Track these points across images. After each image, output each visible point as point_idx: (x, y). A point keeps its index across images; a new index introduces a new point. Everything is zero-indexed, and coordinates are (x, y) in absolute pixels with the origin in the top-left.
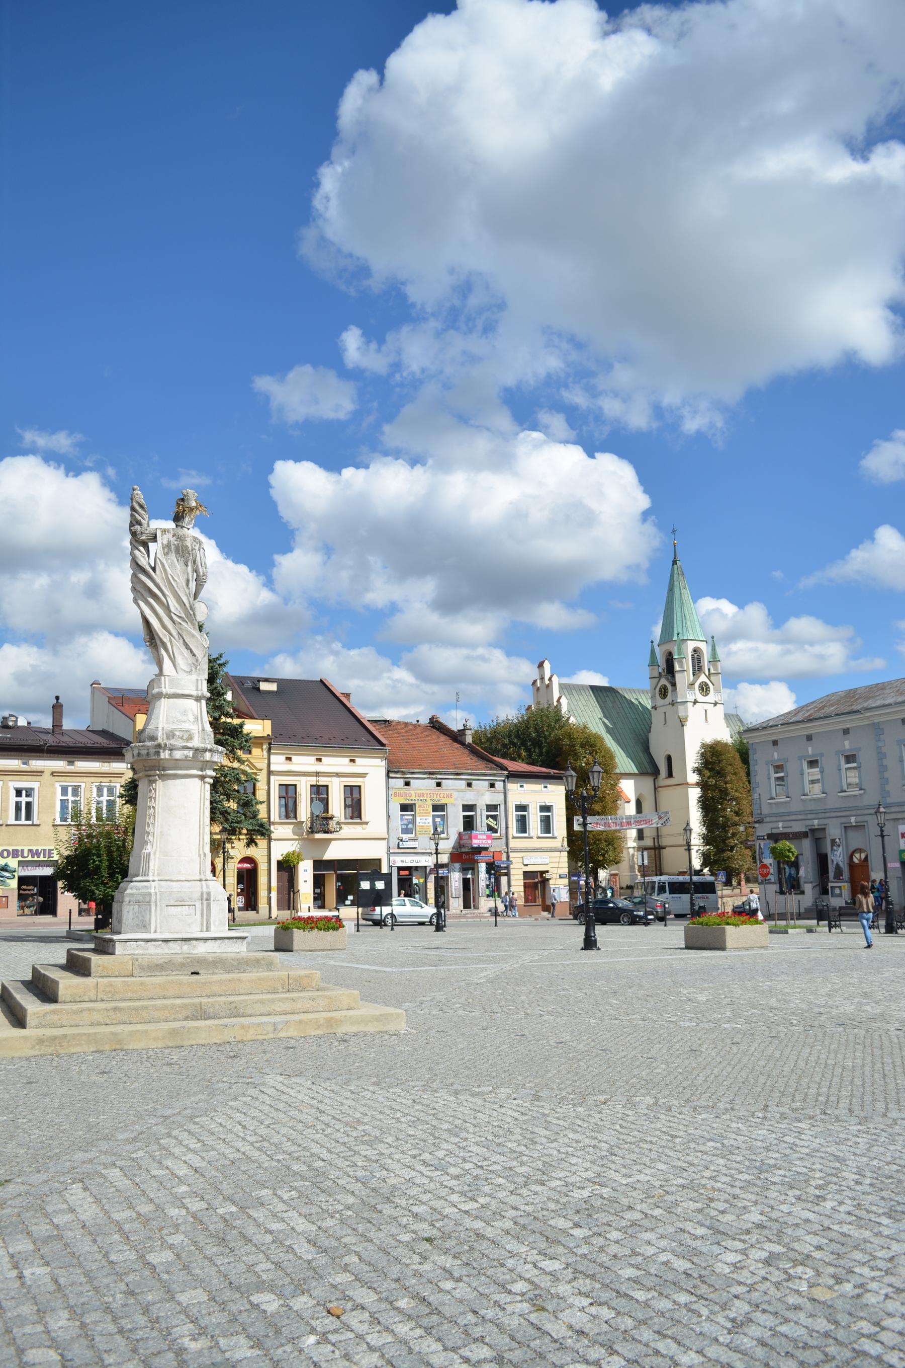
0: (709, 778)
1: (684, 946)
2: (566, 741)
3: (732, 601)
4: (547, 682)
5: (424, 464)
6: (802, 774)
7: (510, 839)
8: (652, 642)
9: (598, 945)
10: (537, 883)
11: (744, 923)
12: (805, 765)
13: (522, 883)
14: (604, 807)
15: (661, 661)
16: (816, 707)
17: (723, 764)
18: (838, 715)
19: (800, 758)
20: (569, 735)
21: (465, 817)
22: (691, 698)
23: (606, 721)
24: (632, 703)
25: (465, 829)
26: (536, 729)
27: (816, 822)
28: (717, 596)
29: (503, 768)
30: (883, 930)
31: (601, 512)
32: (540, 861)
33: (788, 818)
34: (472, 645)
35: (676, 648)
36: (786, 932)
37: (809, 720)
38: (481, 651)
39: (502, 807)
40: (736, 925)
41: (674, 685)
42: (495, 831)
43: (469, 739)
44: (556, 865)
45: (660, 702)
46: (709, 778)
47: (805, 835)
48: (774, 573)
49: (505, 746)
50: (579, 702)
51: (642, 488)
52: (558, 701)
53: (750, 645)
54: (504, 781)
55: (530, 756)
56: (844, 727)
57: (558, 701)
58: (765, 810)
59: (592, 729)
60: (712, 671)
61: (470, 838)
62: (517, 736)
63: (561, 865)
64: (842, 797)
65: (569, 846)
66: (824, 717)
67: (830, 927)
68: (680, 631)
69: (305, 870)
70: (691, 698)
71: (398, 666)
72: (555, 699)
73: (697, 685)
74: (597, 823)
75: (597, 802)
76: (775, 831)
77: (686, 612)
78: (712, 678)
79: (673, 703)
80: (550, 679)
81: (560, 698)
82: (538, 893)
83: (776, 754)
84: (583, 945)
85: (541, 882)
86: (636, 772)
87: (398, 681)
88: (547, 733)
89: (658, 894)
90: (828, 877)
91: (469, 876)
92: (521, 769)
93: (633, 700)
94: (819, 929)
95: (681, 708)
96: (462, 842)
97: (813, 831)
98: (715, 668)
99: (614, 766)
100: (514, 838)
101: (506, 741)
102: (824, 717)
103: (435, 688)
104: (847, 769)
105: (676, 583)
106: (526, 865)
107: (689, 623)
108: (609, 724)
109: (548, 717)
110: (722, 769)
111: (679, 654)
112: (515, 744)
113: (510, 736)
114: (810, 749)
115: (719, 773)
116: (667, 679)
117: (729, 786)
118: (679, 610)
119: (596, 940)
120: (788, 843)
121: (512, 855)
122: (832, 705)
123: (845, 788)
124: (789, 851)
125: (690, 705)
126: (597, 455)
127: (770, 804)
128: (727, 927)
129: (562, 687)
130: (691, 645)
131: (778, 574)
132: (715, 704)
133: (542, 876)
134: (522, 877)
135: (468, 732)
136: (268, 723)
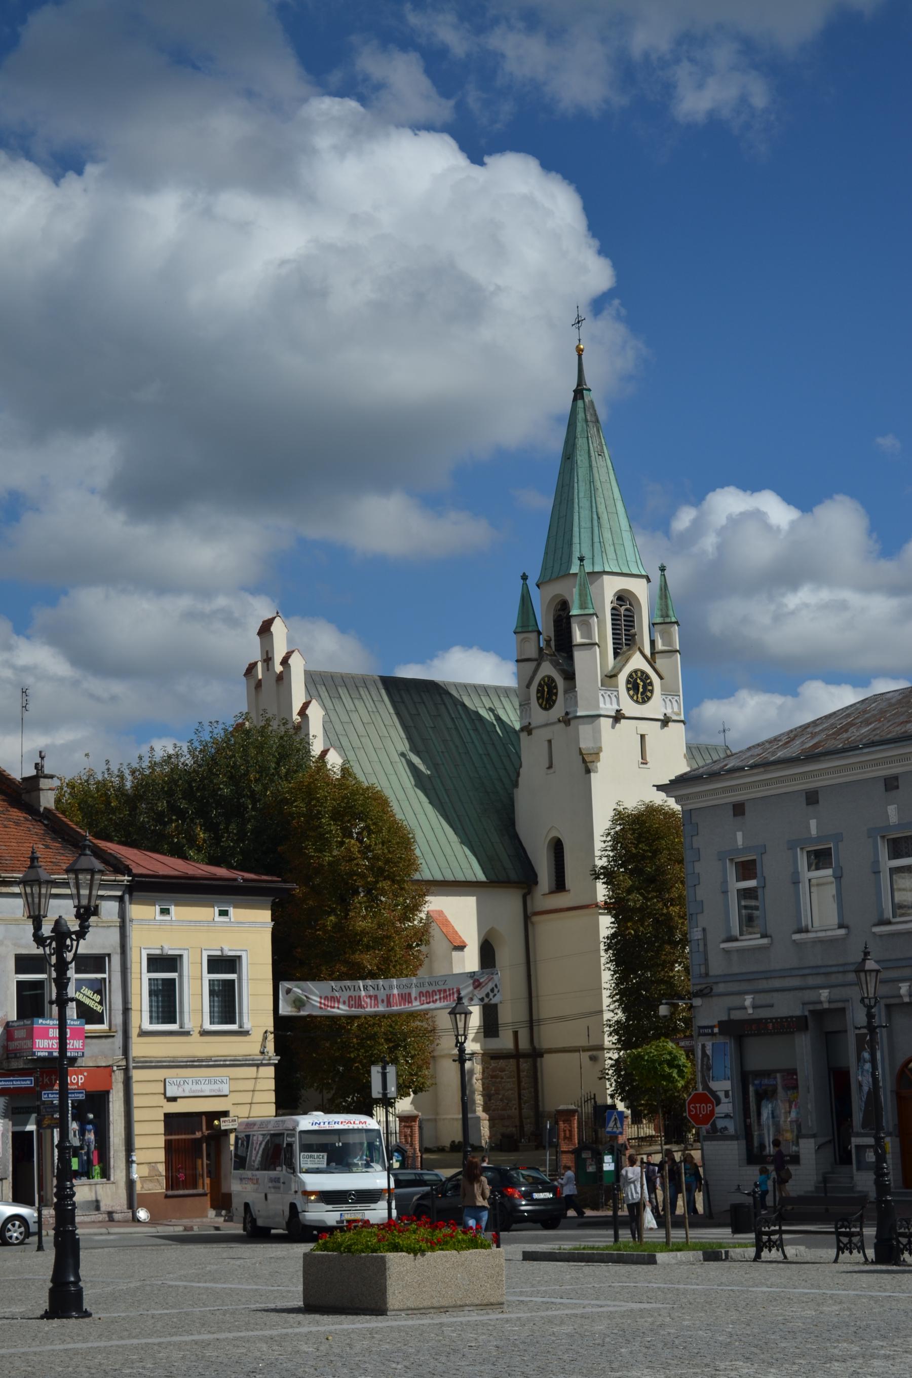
0: (629, 891)
1: (300, 1304)
2: (300, 806)
3: (789, 498)
4: (278, 668)
5: (80, 172)
6: (796, 882)
8: (524, 577)
9: (86, 1306)
10: (198, 1142)
11: (434, 1245)
12: (803, 861)
13: (161, 1141)
14: (386, 960)
15: (544, 620)
16: (832, 726)
17: (663, 858)
18: (873, 744)
19: (792, 846)
20: (309, 792)
21: (20, 984)
22: (607, 707)
23: (416, 760)
24: (480, 718)
25: (21, 1015)
26: (231, 777)
27: (824, 994)
28: (751, 486)
29: (119, 867)
30: (871, 1253)
31: (498, 288)
32: (207, 1089)
33: (764, 984)
34: (205, 591)
35: (576, 591)
36: (652, 1260)
37: (811, 756)
38: (221, 601)
39: (116, 960)
40: (415, 1251)
41: (570, 676)
42: (97, 1018)
43: (47, 800)
44: (247, 1098)
45: (538, 716)
46: (629, 891)
47: (796, 1025)
48: (880, 440)
49: (159, 818)
50: (354, 717)
51: (596, 243)
52: (303, 713)
53: (825, 595)
54: (121, 899)
55: (217, 839)
57: (303, 713)
58: (717, 967)
59: (361, 777)
60: (660, 646)
61: (30, 1036)
62: (189, 794)
63: (259, 1097)
65: (277, 1051)
66: (844, 750)
67: (760, 1246)
68: (587, 553)
70: (607, 707)
71: (28, 638)
72: (296, 707)
73: (622, 678)
74: (333, 999)
75: (368, 948)
76: (737, 1015)
77: (602, 508)
78: (660, 662)
79: (567, 720)
80: (285, 662)
81: (306, 706)
82: (203, 1163)
83: (739, 835)
84: (45, 1305)
85: (207, 1139)
86: (481, 877)
87: (25, 669)
88: (257, 788)
90: (851, 1126)
91: (31, 1127)
92: (163, 871)
93: (483, 712)
94: (735, 1252)
95: (584, 730)
96: (13, 1045)
97: (820, 1015)
98: (668, 640)
99: (411, 864)
100: (143, 1034)
101: (162, 805)
102: (844, 750)
103: (117, 687)
104: (894, 871)
105: (581, 442)
107: (607, 535)
108: (422, 768)
109: (260, 748)
110: (660, 871)
111: (583, 606)
112: (181, 814)
113: (170, 793)
114: (813, 823)
115: (651, 880)
116: (556, 664)
117: (674, 910)
118: (585, 503)
119: (79, 1293)
120: (671, 1045)
121: (136, 1075)
122: (867, 722)
123: (888, 913)
124: (672, 1063)
125: (606, 723)
126: (487, 159)
127: (726, 952)
128: (390, 1256)
129: (313, 680)
130: (611, 586)
131: (888, 442)
132: (665, 722)
133: (210, 1125)
134: (160, 1128)
135: (44, 783)
136: (811, 821)
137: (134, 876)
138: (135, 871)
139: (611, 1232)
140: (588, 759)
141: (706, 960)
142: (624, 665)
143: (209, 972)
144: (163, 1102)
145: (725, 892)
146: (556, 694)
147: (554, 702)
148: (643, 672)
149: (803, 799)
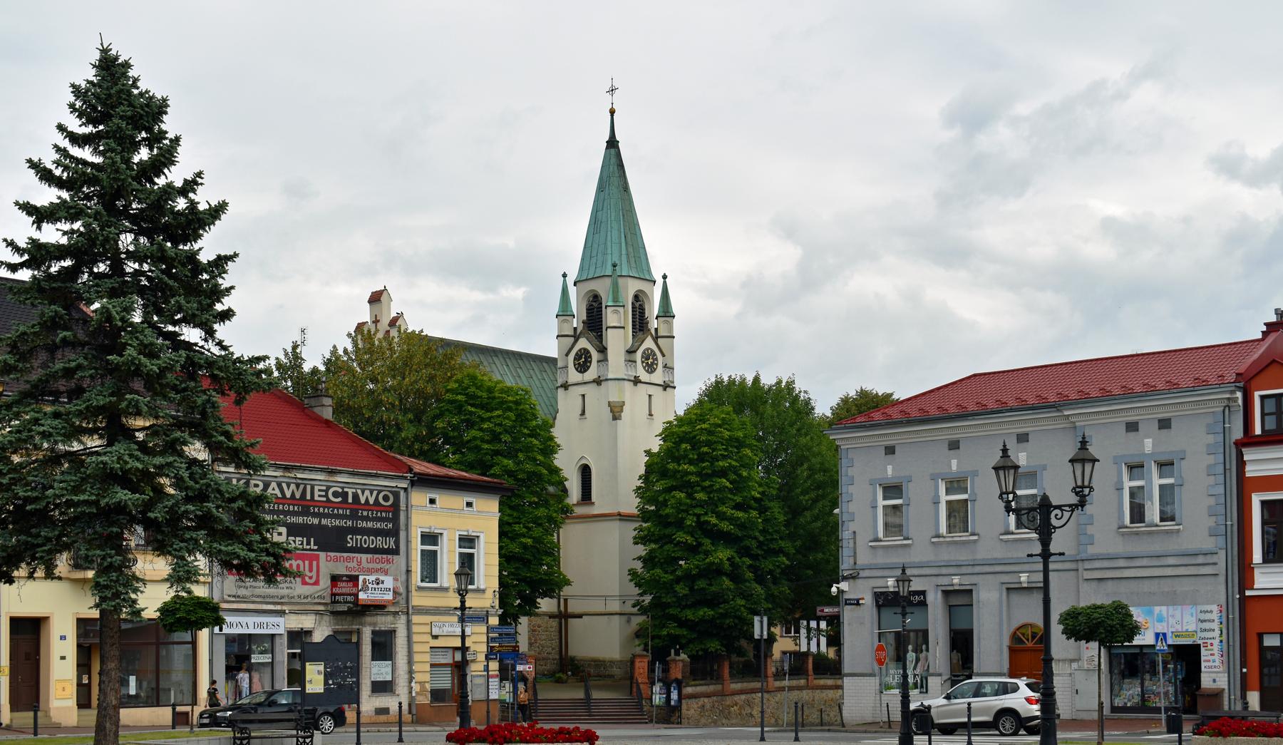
7: (414, 593)
8: (565, 276)
27: (956, 580)
41: (603, 350)
56: (1161, 416)
64: (1007, 541)
69: (63, 638)
89: (1027, 685)
106: (436, 637)
121: (415, 619)
137: (415, 474)
138: (415, 470)
139: (927, 737)
140: (616, 410)
141: (855, 553)
142: (640, 345)
143: (422, 544)
144: (429, 638)
145: (875, 507)
146: (590, 362)
147: (589, 367)
148: (652, 351)
149: (946, 446)
